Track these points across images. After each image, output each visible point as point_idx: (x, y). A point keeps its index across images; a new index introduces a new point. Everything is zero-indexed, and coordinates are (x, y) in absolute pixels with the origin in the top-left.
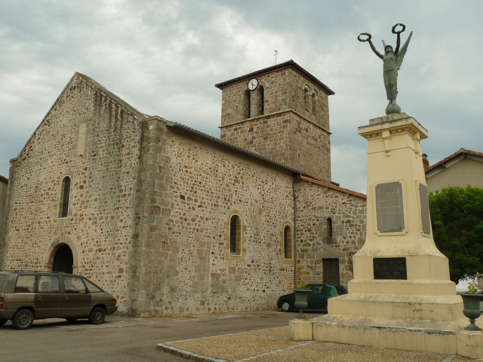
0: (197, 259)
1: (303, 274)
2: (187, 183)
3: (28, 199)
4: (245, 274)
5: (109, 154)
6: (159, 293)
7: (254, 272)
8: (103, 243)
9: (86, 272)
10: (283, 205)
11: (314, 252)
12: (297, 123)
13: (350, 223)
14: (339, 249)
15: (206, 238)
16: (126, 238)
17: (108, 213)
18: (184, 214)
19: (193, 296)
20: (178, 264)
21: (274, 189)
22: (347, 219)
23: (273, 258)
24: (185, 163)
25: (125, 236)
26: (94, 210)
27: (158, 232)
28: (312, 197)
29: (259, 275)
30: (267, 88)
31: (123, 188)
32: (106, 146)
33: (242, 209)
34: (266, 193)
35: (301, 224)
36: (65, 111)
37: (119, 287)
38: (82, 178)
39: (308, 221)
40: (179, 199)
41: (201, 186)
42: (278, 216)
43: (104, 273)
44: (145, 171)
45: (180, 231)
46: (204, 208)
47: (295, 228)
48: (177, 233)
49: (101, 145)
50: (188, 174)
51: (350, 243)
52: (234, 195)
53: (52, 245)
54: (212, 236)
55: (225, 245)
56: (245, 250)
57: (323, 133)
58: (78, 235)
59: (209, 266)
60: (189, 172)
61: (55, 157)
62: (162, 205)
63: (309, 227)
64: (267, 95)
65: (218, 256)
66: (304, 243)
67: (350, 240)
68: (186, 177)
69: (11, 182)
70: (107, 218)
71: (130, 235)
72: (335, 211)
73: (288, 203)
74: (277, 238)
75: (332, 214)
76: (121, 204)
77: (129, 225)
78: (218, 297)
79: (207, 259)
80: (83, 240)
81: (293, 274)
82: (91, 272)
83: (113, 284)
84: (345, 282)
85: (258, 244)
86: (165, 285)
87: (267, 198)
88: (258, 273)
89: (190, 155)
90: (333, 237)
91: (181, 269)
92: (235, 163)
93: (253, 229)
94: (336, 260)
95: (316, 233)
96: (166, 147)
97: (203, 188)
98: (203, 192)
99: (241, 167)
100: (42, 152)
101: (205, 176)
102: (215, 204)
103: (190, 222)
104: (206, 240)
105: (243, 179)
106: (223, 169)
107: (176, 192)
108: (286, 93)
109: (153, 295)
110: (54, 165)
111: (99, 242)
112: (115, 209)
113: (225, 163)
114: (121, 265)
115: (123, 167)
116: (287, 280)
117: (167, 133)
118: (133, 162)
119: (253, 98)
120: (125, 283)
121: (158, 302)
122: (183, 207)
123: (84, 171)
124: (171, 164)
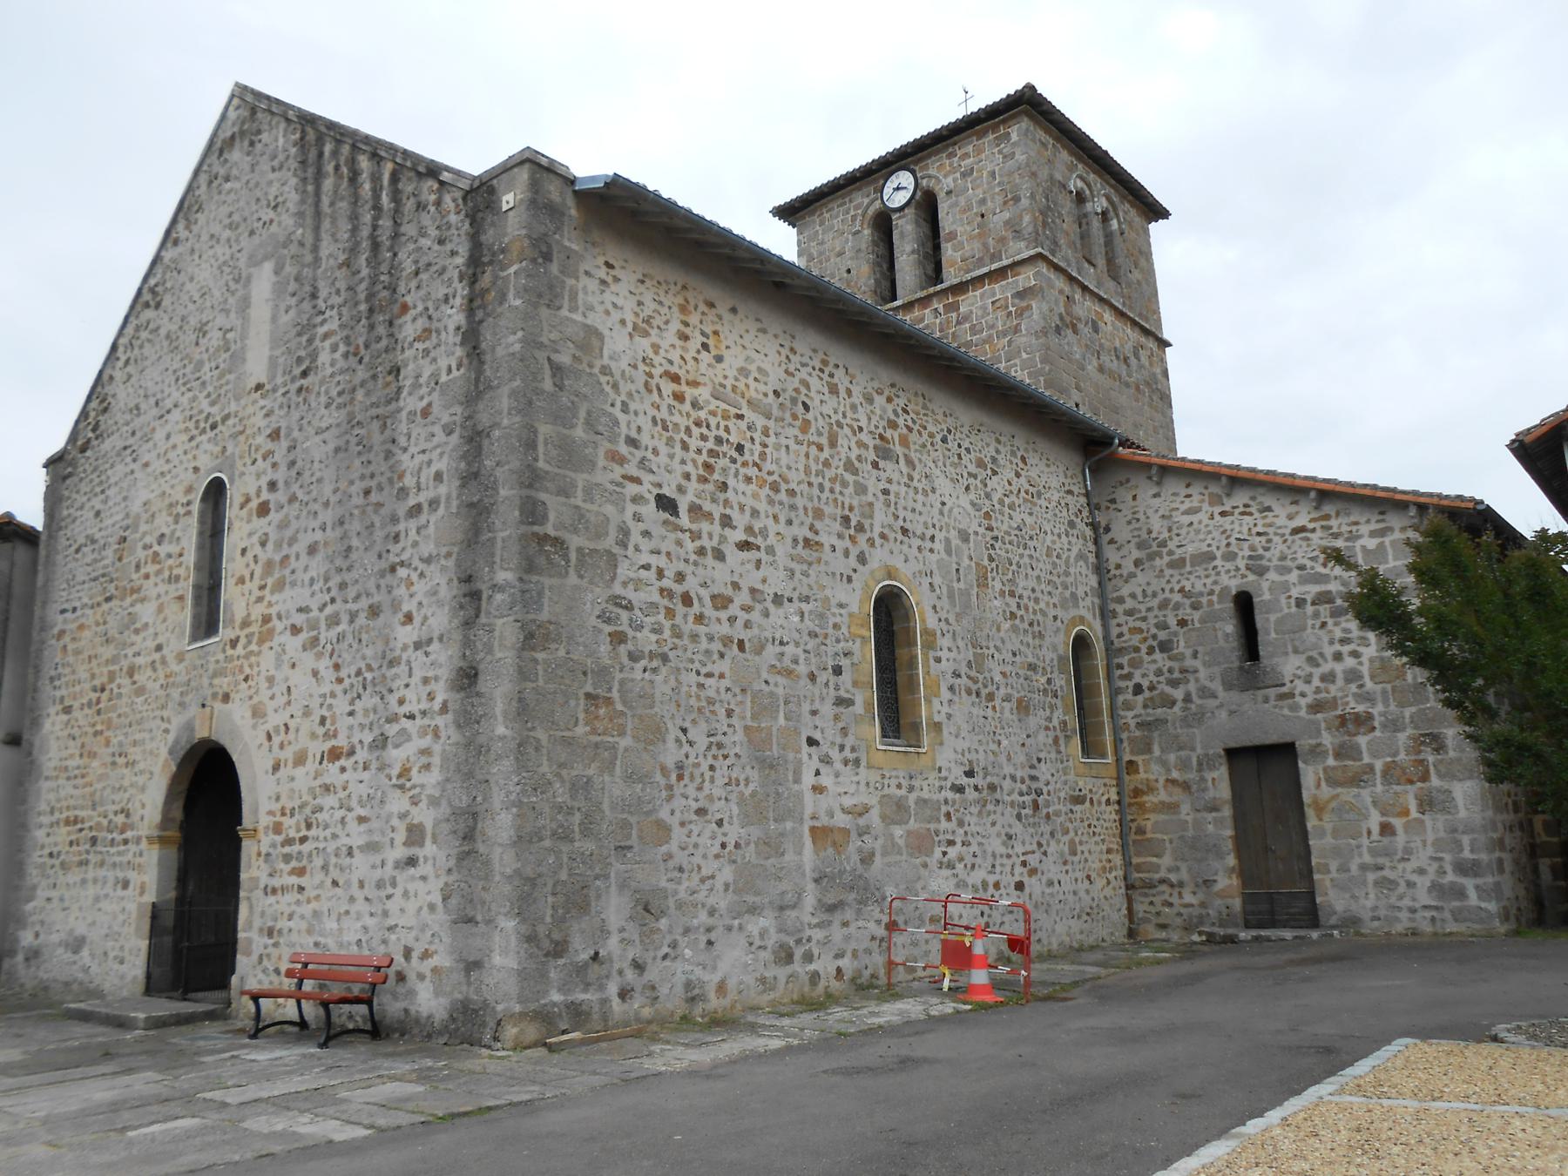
0: (748, 768)
1: (1154, 811)
2: (685, 447)
3: (97, 587)
4: (944, 824)
5: (355, 354)
6: (583, 925)
7: (980, 812)
8: (344, 723)
9: (287, 849)
10: (1058, 557)
11: (1190, 726)
12: (1062, 299)
13: (1331, 601)
14: (1295, 708)
15: (781, 680)
16: (428, 689)
17: (358, 597)
18: (680, 577)
19: (741, 928)
20: (664, 794)
21: (1023, 494)
22: (1314, 589)
23: (1042, 755)
24: (671, 362)
25: (426, 681)
26: (307, 592)
27: (562, 653)
28: (1165, 523)
29: (998, 827)
30: (949, 193)
31: (409, 481)
32: (342, 326)
33: (914, 566)
34: (997, 506)
35: (1131, 624)
36: (205, 237)
37: (411, 906)
38: (264, 472)
39: (1156, 612)
40: (649, 510)
41: (745, 464)
42: (1046, 598)
43: (350, 853)
44: (490, 388)
45: (666, 649)
46: (762, 555)
47: (1106, 637)
48: (652, 656)
49: (325, 328)
50: (687, 407)
51: (1340, 682)
52: (879, 506)
53: (171, 752)
54: (802, 669)
55: (859, 708)
56: (937, 727)
57: (1143, 339)
58: (256, 700)
59: (799, 797)
60: (688, 402)
61: (176, 415)
62: (576, 531)
63: (1162, 635)
64: (948, 219)
65: (835, 754)
66: (1147, 694)
67: (1339, 668)
68: (677, 418)
69: (50, 537)
70: (353, 616)
71: (445, 673)
72: (1264, 562)
73: (1075, 550)
74: (1049, 681)
75: (1251, 577)
76: (403, 549)
77: (436, 635)
78: (845, 924)
79: (791, 767)
80: (274, 720)
81: (1114, 816)
82: (307, 847)
83: (389, 897)
84: (1329, 831)
85: (984, 703)
86: (613, 888)
87: (1002, 525)
88: (992, 817)
89: (688, 331)
90: (1265, 661)
91: (678, 814)
92: (876, 384)
93: (961, 644)
94: (1286, 751)
95: (1195, 655)
96: (580, 285)
97: (752, 472)
98: (753, 487)
99: (896, 401)
100: (137, 407)
101: (760, 422)
102: (806, 541)
103: (709, 611)
104: (781, 686)
105: (908, 448)
106: (832, 402)
107: (637, 481)
108: (1017, 199)
109: (556, 936)
110: (174, 447)
111: (328, 722)
112: (382, 574)
113: (835, 380)
114: (414, 811)
115: (405, 393)
116: (1097, 838)
117: (584, 229)
118: (443, 363)
119: (902, 235)
120: (431, 891)
121: (581, 969)
122: (672, 548)
123: (270, 445)
124: (606, 361)
